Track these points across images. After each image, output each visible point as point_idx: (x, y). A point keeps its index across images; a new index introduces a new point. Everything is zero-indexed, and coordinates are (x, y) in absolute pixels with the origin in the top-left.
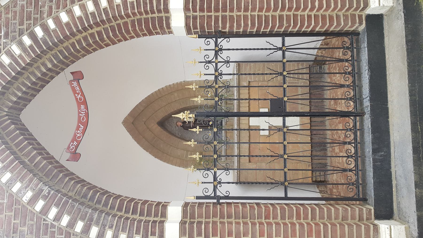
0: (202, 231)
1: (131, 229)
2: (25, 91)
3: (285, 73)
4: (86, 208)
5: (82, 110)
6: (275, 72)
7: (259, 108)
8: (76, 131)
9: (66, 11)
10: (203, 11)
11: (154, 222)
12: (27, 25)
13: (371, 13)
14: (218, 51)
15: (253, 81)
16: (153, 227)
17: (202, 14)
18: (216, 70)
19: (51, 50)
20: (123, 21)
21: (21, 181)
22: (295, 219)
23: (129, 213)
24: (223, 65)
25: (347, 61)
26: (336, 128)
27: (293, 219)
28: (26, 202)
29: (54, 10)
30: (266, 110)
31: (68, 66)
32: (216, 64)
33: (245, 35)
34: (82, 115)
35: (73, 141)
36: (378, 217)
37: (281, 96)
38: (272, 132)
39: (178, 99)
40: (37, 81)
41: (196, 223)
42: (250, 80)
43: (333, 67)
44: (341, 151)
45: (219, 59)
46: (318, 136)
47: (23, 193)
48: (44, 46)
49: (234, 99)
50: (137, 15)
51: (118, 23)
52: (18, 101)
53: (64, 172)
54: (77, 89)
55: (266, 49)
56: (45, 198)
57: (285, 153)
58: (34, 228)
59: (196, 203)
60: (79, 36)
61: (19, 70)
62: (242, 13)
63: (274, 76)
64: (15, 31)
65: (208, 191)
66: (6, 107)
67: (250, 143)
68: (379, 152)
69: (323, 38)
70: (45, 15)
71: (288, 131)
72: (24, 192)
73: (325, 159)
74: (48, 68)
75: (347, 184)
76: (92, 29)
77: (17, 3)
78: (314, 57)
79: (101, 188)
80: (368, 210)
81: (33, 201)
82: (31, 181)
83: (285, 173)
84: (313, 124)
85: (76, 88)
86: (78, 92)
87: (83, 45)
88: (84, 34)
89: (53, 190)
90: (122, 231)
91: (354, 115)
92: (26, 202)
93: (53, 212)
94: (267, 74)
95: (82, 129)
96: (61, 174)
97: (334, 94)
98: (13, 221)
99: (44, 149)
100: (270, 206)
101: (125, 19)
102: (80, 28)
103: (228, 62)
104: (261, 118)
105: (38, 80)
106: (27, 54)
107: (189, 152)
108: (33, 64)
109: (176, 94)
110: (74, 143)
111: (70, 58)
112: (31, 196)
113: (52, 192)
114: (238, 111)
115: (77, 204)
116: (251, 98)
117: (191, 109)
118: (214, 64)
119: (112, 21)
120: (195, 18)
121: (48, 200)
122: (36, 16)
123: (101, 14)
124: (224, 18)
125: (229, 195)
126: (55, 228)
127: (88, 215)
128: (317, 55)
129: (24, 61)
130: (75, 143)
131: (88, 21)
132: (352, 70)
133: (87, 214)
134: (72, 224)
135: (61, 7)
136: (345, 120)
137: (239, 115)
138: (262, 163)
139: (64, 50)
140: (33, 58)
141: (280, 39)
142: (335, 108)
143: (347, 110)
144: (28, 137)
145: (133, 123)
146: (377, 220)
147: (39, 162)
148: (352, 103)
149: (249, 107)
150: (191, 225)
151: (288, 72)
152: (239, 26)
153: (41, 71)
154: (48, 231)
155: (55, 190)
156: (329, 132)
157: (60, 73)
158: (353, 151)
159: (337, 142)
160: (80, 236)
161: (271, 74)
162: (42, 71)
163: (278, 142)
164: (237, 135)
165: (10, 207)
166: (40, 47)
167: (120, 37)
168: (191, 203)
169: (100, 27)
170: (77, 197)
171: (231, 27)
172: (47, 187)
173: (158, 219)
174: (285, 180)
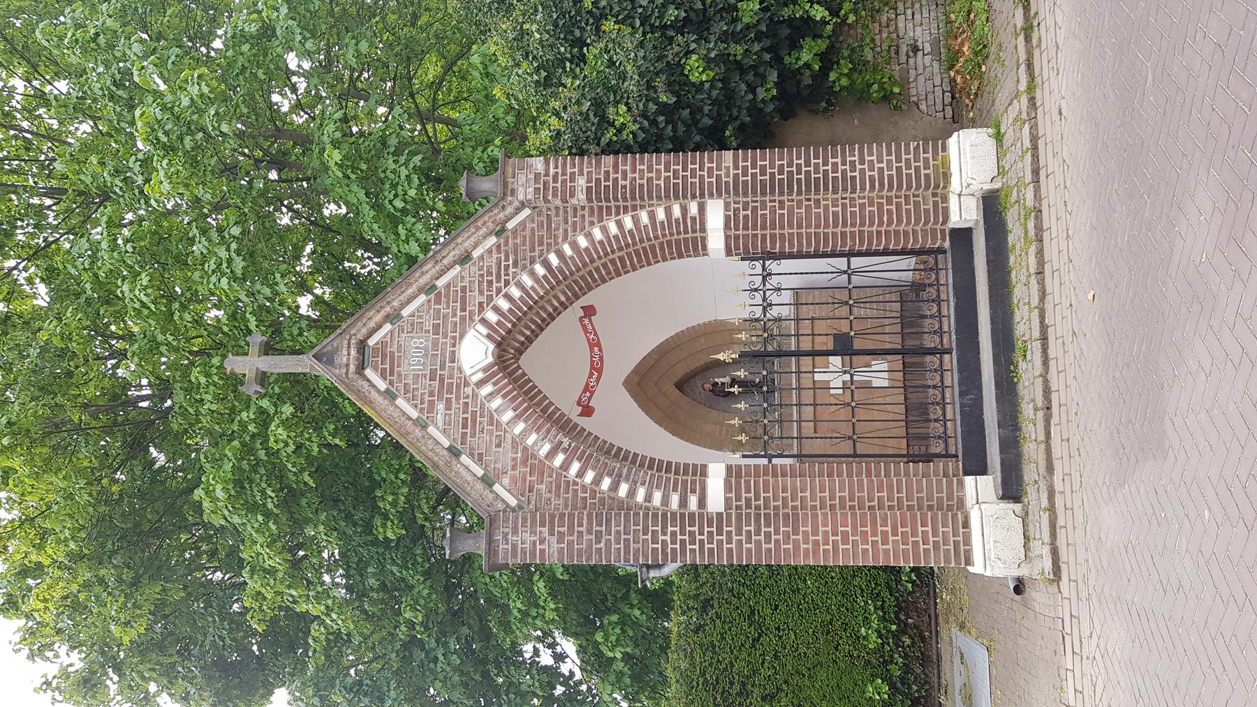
10: (753, 235)
14: (766, 276)
17: (745, 233)
18: (764, 299)
29: (570, 234)
32: (764, 292)
33: (800, 255)
35: (584, 392)
56: (565, 451)
62: (795, 231)
67: (815, 405)
70: (560, 240)
81: (551, 454)
82: (548, 432)
84: (908, 377)
88: (604, 260)
93: (575, 467)
98: (529, 478)
103: (779, 289)
109: (702, 340)
113: (573, 445)
118: (762, 292)
120: (737, 237)
122: (549, 241)
123: (626, 237)
124: (773, 236)
129: (537, 294)
130: (588, 394)
131: (611, 245)
152: (791, 245)
153: (552, 305)
166: (555, 277)
171: (782, 246)
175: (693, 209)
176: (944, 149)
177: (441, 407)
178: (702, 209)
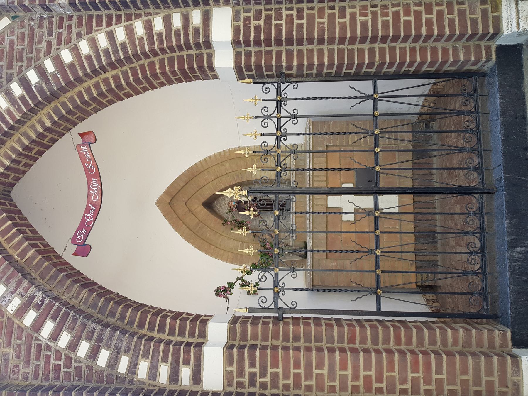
0: (255, 360)
1: (156, 354)
2: (14, 159)
3: (377, 132)
4: (94, 324)
5: (93, 185)
6: (362, 131)
7: (342, 183)
8: (86, 214)
9: (70, 48)
11: (189, 344)
12: (17, 68)
13: (504, 44)
14: (280, 101)
15: (333, 146)
16: (187, 352)
17: (258, 49)
18: (279, 128)
19: (50, 103)
20: (149, 60)
22: (392, 343)
23: (154, 330)
24: (289, 121)
25: (469, 113)
26: (452, 211)
27: (389, 344)
28: (12, 312)
30: (351, 185)
31: (75, 124)
34: (94, 192)
35: (80, 228)
37: (371, 164)
38: (359, 216)
39: (231, 171)
40: (30, 146)
41: (248, 346)
42: (328, 144)
43: (447, 124)
44: (458, 245)
45: (283, 113)
46: (425, 222)
47: (7, 301)
50: (168, 53)
51: (140, 64)
52: (6, 172)
53: (67, 271)
54: (88, 156)
55: (350, 98)
56: (38, 307)
57: (377, 248)
58: (22, 350)
59: (249, 317)
60: (89, 83)
61: (6, 129)
63: (362, 135)
64: (2, 76)
65: (265, 301)
68: (517, 247)
69: (433, 80)
70: (42, 55)
71: (382, 215)
72: (9, 300)
73: (435, 255)
74: (46, 126)
75: (469, 293)
76: (105, 73)
77: (4, 38)
78: (417, 116)
79: (118, 294)
80: (502, 332)
81: (22, 311)
82: (19, 284)
83: (378, 276)
85: (86, 155)
86: (88, 160)
87: (93, 94)
89: (49, 296)
91: (479, 192)
92: (12, 312)
93: (49, 327)
94: (351, 133)
95: (94, 211)
96: (62, 274)
97: (448, 163)
99: (41, 238)
100: (355, 323)
101: (151, 58)
102: (88, 71)
104: (343, 196)
105: (32, 144)
106: (17, 107)
107: (245, 244)
108: (25, 122)
109: (227, 165)
110: (82, 231)
111: (77, 114)
112: (19, 305)
113: (47, 300)
114: (311, 187)
115: (82, 317)
118: (275, 120)
119: (132, 60)
121: (41, 310)
125: (296, 307)
126: (50, 350)
127: (96, 334)
132: (477, 126)
133: (94, 331)
134: (73, 346)
135: (63, 43)
136: (464, 199)
137: (314, 192)
138: (346, 259)
139: (68, 103)
140: (25, 113)
141: (370, 83)
142: (450, 182)
143: (467, 185)
144: (19, 221)
146: (516, 348)
147: (33, 258)
148: (475, 174)
150: (241, 351)
151: (381, 131)
153: (36, 131)
154: (41, 354)
155: (52, 297)
156: (438, 217)
157: (64, 134)
158: (478, 244)
159: (452, 231)
160: (84, 363)
161: (356, 133)
162: (38, 132)
163: (368, 231)
164: (309, 220)
167: (145, 84)
168: (242, 317)
169: (117, 70)
170: (83, 307)
172: (41, 292)
173: (194, 340)
174: (378, 287)
178: (206, 18)
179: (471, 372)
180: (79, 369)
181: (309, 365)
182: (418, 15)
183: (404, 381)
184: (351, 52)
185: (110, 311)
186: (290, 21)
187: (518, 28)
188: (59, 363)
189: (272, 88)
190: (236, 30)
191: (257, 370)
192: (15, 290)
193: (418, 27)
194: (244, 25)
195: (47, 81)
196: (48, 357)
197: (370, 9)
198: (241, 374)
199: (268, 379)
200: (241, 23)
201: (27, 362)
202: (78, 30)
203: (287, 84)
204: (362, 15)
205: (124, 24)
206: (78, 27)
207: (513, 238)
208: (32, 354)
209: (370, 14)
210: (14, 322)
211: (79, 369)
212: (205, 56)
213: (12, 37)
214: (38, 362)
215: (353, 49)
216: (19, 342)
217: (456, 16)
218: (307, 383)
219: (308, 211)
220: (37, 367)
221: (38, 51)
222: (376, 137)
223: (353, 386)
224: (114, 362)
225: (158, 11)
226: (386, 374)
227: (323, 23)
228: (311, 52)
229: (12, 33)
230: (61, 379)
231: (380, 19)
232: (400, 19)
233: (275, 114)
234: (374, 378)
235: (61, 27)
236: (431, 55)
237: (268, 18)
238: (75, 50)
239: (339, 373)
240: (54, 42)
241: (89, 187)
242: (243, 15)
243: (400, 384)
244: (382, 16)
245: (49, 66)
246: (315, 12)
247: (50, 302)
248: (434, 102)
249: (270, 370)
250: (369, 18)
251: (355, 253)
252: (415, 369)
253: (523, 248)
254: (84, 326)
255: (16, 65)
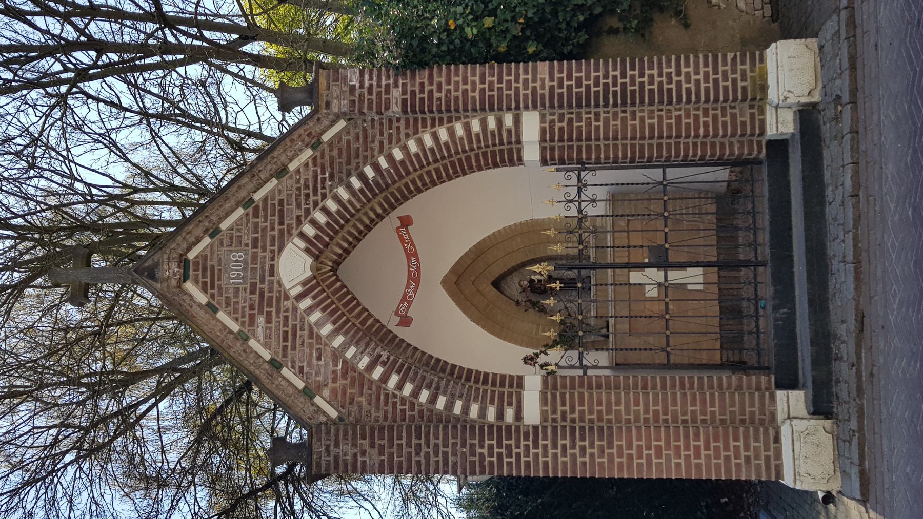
1: (484, 398)
18: (580, 211)
21: (357, 344)
32: (580, 204)
35: (402, 301)
36: (779, 386)
45: (584, 197)
48: (376, 189)
49: (608, 247)
56: (384, 364)
66: (330, 261)
70: (376, 153)
78: (725, 184)
81: (371, 367)
90: (474, 400)
93: (394, 379)
116: (632, 244)
117: (549, 259)
118: (577, 204)
121: (387, 366)
128: (729, 182)
134: (416, 394)
137: (614, 266)
141: (661, 170)
145: (455, 283)
149: (628, 256)
153: (369, 218)
165: (345, 374)
175: (508, 120)
176: (762, 60)
177: (261, 320)
178: (517, 121)
179: (737, 405)
180: (421, 412)
181: (609, 403)
182: (697, 117)
183: (684, 413)
184: (642, 146)
185: (441, 369)
186: (589, 124)
187: (777, 130)
188: (404, 407)
189: (574, 176)
190: (543, 131)
191: (567, 408)
192: (365, 350)
193: (697, 129)
194: (550, 127)
195: (382, 175)
196: (395, 404)
197: (657, 113)
198: (554, 411)
199: (576, 415)
200: (547, 125)
201: (378, 408)
202: (406, 131)
203: (587, 172)
204: (650, 118)
205: (446, 125)
206: (406, 128)
207: (777, 302)
208: (381, 401)
209: (656, 118)
210: (364, 376)
211: (421, 412)
212: (515, 151)
213: (348, 137)
214: (386, 408)
215: (644, 144)
216: (370, 392)
217: (728, 119)
218: (607, 417)
219: (609, 245)
220: (386, 412)
221: (372, 149)
222: (666, 218)
223: (644, 418)
224: (450, 405)
225: (475, 114)
226: (670, 408)
227: (616, 125)
228: (607, 146)
229: (348, 133)
230: (407, 421)
231: (665, 121)
232: (681, 121)
233: (577, 199)
234: (661, 412)
235: (390, 128)
236: (711, 149)
237: (570, 121)
238: (405, 149)
239: (633, 408)
240: (386, 141)
241: (408, 265)
242: (549, 118)
243: (682, 415)
244: (667, 119)
245: (383, 163)
246: (610, 115)
247: (394, 359)
248: (741, 172)
249: (577, 408)
250: (655, 121)
251: (648, 318)
252: (694, 404)
253: (785, 310)
254: (424, 378)
255: (354, 162)
